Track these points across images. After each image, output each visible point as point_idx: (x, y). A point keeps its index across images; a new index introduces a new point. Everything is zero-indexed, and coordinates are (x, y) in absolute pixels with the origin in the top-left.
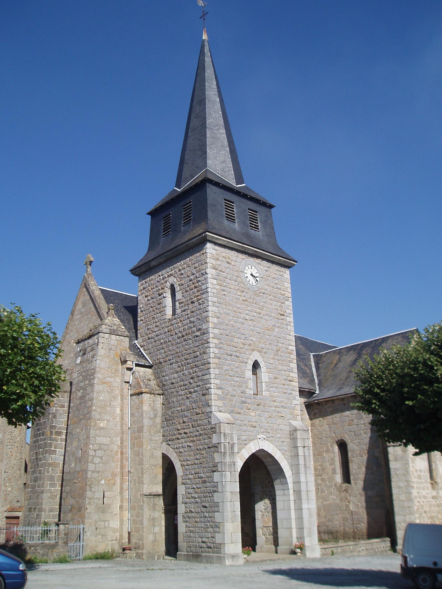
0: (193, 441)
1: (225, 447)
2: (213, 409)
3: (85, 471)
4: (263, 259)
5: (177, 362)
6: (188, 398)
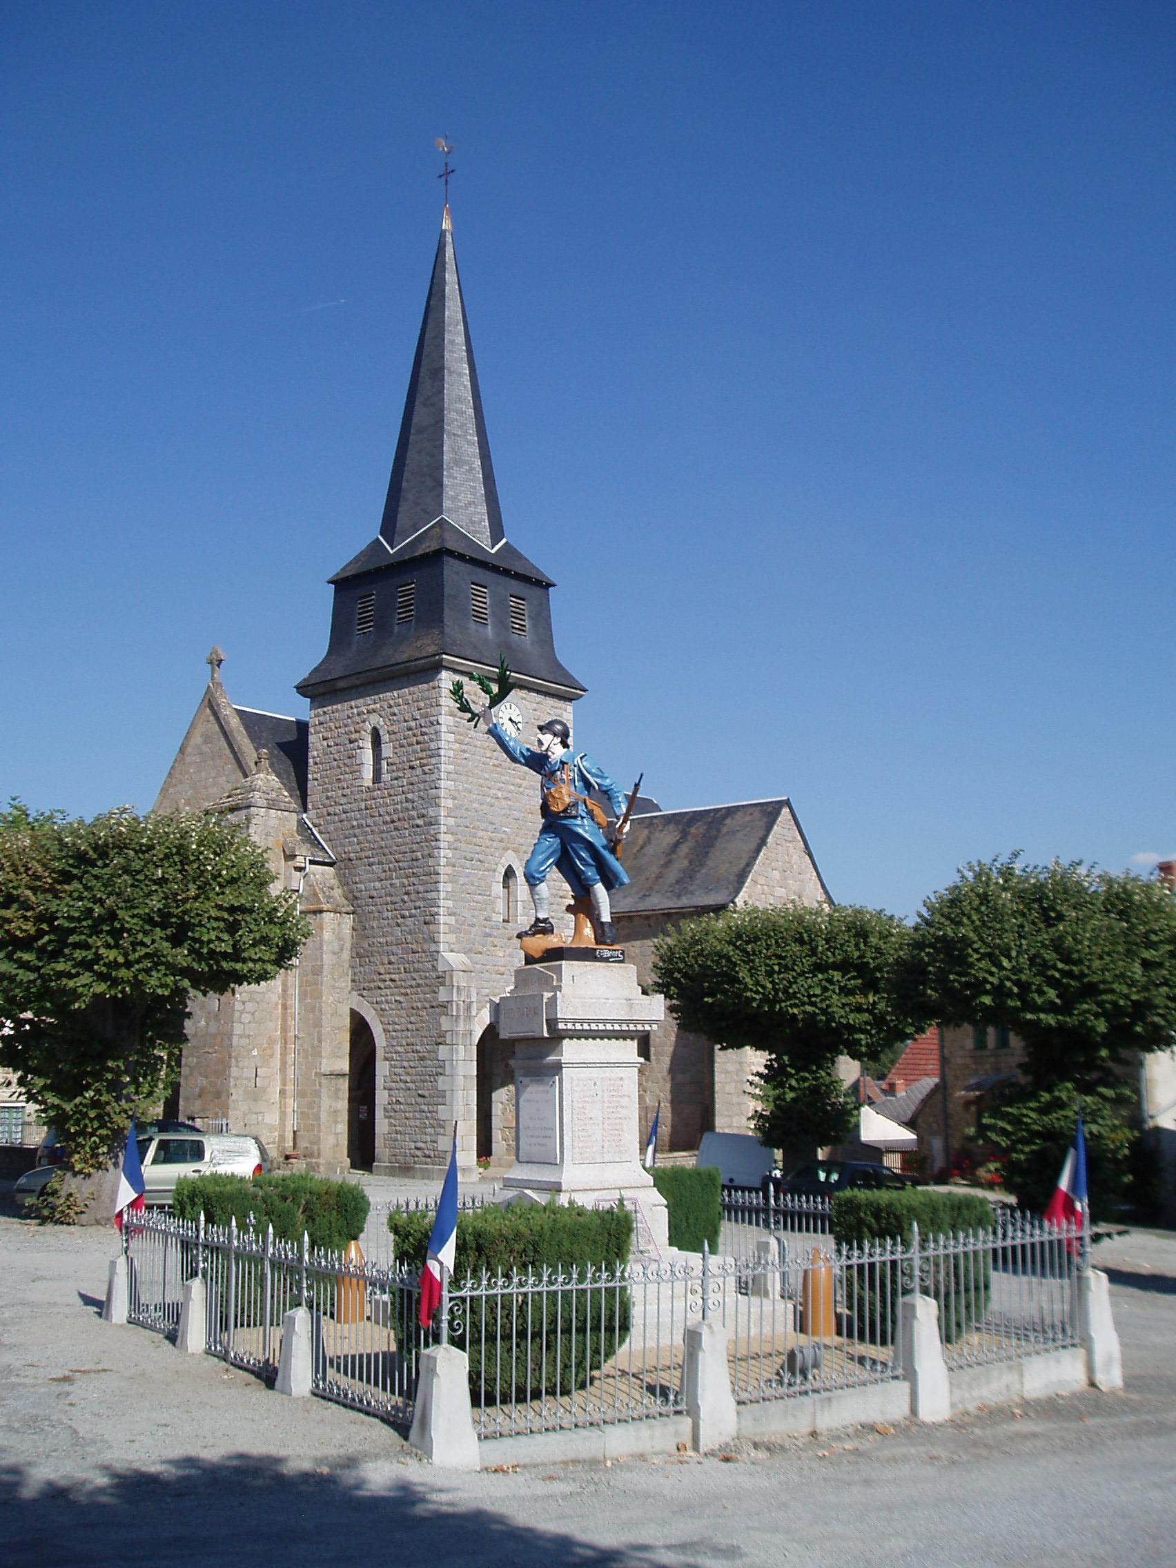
0: (407, 994)
1: (458, 1008)
2: (442, 947)
3: (230, 1035)
4: (530, 690)
5: (380, 863)
6: (398, 925)
